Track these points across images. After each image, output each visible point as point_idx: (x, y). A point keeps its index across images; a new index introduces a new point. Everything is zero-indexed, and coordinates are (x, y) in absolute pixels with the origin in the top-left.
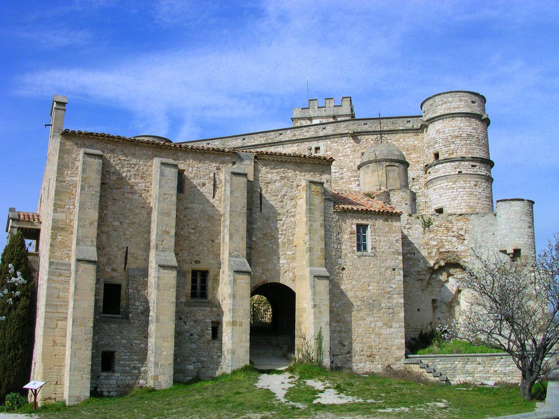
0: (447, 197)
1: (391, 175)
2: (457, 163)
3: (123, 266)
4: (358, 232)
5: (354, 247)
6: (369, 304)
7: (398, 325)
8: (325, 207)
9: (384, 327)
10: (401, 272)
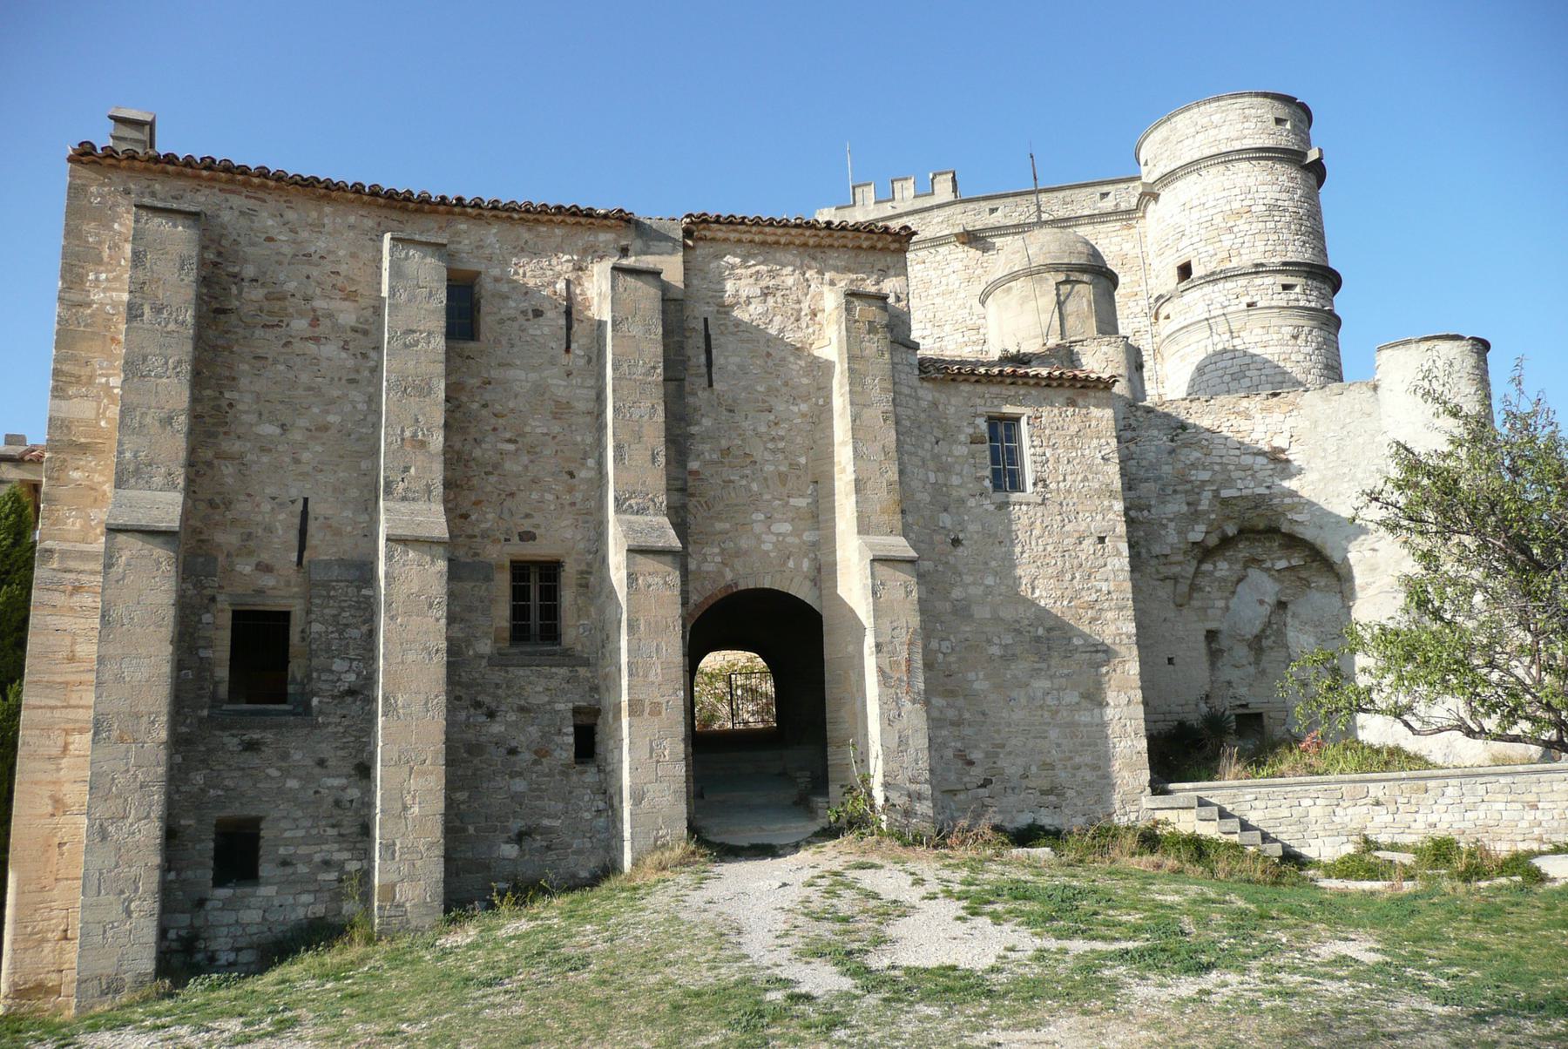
0: (1220, 373)
1: (1070, 307)
2: (1243, 281)
3: (294, 557)
4: (993, 437)
5: (984, 478)
6: (1038, 639)
7: (1123, 700)
8: (894, 364)
9: (1084, 703)
10: (1124, 547)
